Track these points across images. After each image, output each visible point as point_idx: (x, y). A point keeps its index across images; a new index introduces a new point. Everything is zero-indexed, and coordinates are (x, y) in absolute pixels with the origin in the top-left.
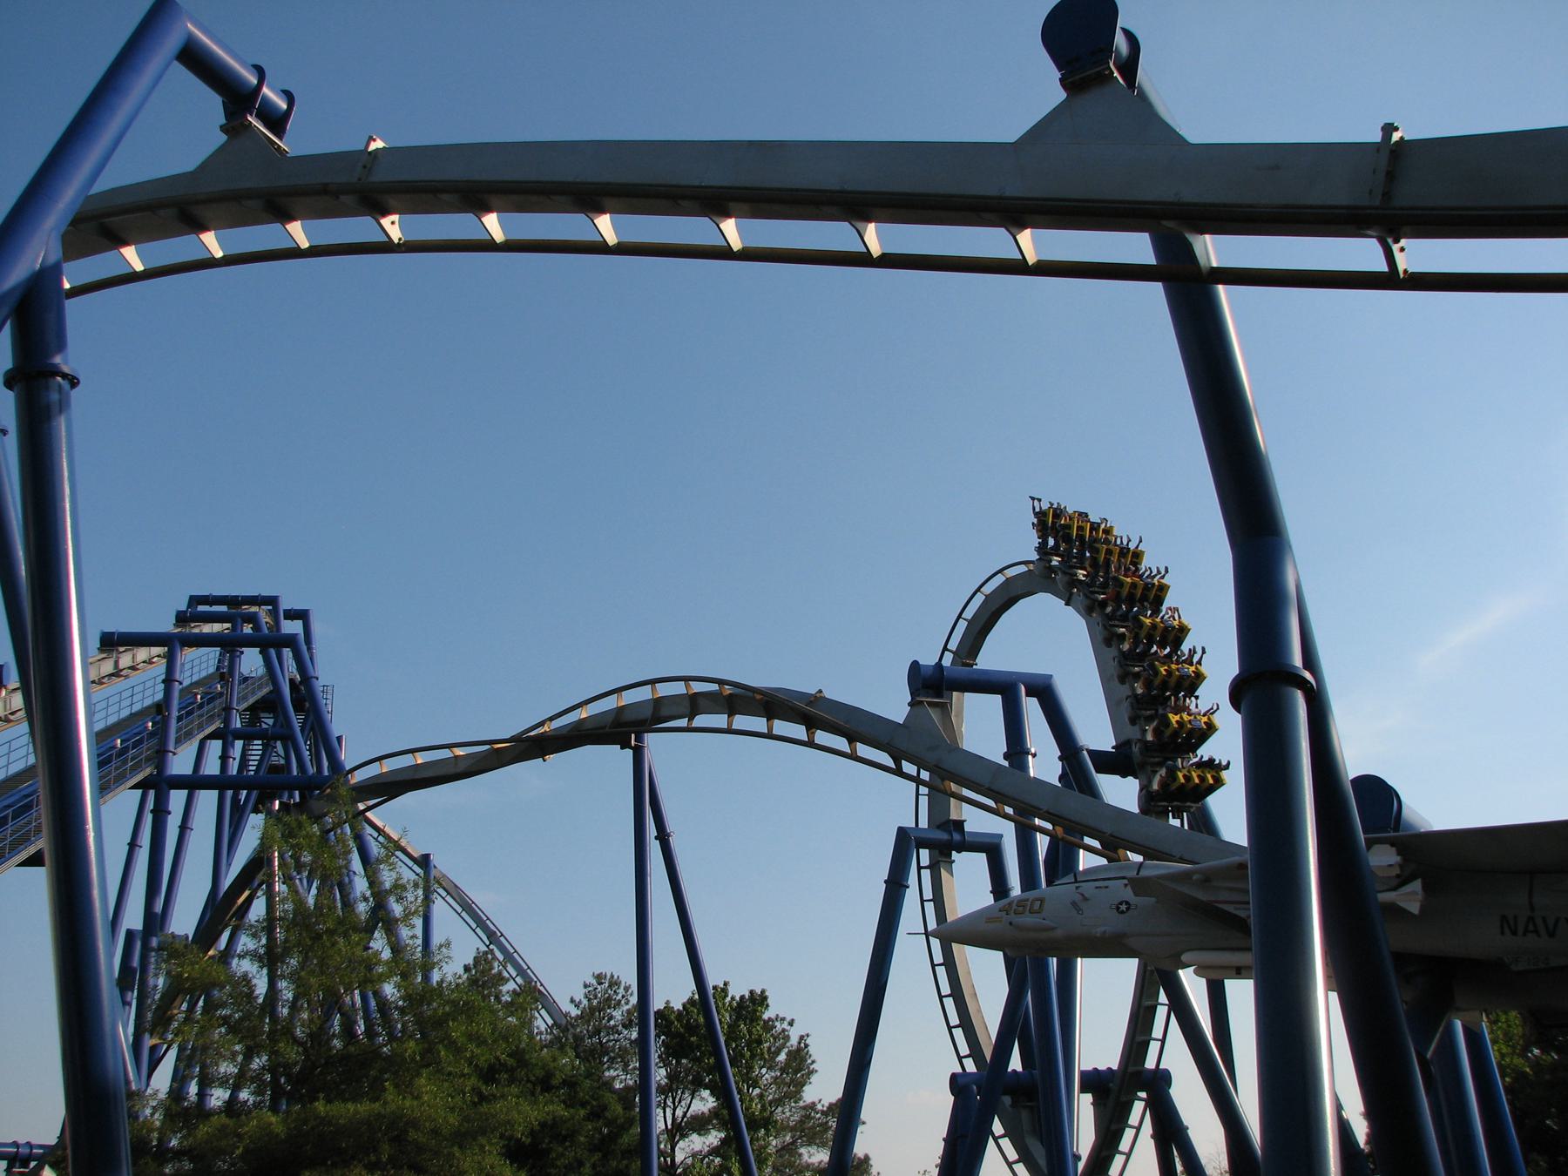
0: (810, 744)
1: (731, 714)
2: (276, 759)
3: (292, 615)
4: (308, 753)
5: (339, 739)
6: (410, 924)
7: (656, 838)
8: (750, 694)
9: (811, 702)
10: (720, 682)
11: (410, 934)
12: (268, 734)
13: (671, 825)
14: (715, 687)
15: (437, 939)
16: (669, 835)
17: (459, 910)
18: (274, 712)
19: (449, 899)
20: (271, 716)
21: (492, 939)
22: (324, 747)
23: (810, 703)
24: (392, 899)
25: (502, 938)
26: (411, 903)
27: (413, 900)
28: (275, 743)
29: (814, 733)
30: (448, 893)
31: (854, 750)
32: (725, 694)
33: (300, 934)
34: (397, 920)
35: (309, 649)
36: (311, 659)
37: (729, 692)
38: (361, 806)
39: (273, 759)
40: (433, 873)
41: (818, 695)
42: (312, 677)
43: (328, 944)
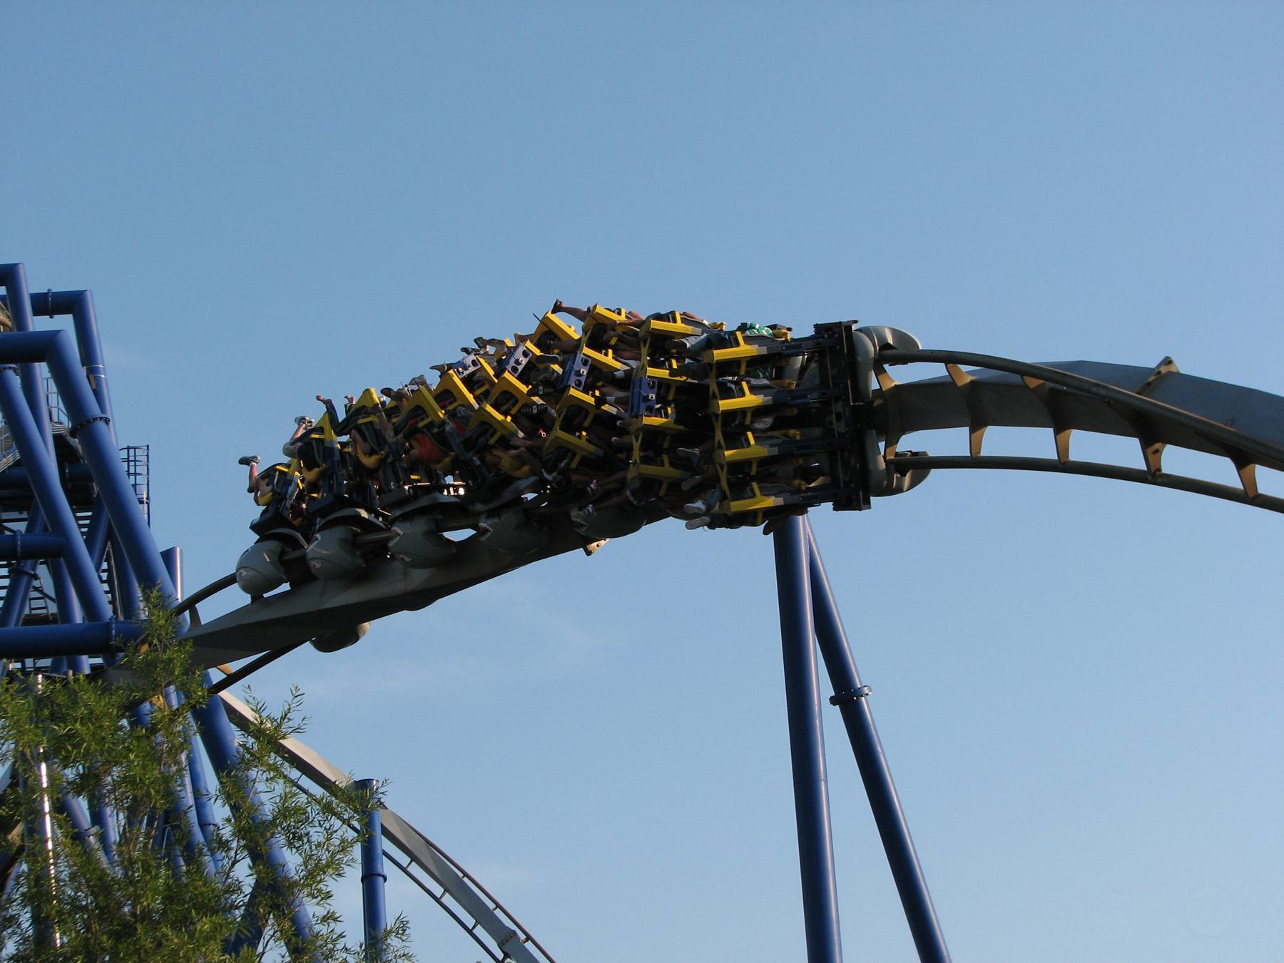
0: (1153, 476)
1: (977, 425)
2: (41, 603)
3: (48, 304)
4: (106, 587)
5: (168, 556)
6: (320, 891)
7: (834, 701)
8: (1015, 378)
9: (1149, 384)
10: (950, 359)
11: (321, 912)
12: (15, 546)
13: (862, 671)
14: (936, 371)
15: (389, 918)
16: (859, 693)
17: (438, 890)
18: (27, 509)
19: (415, 869)
20: (25, 515)
21: (506, 948)
22: (135, 570)
23: (1147, 388)
24: (281, 839)
25: (529, 945)
26: (318, 845)
27: (322, 839)
28: (34, 568)
29: (1157, 452)
30: (414, 859)
31: (1250, 482)
32: (960, 383)
33: (88, 929)
34: (293, 885)
35: (92, 371)
36: (98, 393)
37: (969, 379)
38: (216, 675)
39: (35, 604)
40: (380, 818)
41: (1164, 370)
42: (95, 419)
43: (149, 944)
